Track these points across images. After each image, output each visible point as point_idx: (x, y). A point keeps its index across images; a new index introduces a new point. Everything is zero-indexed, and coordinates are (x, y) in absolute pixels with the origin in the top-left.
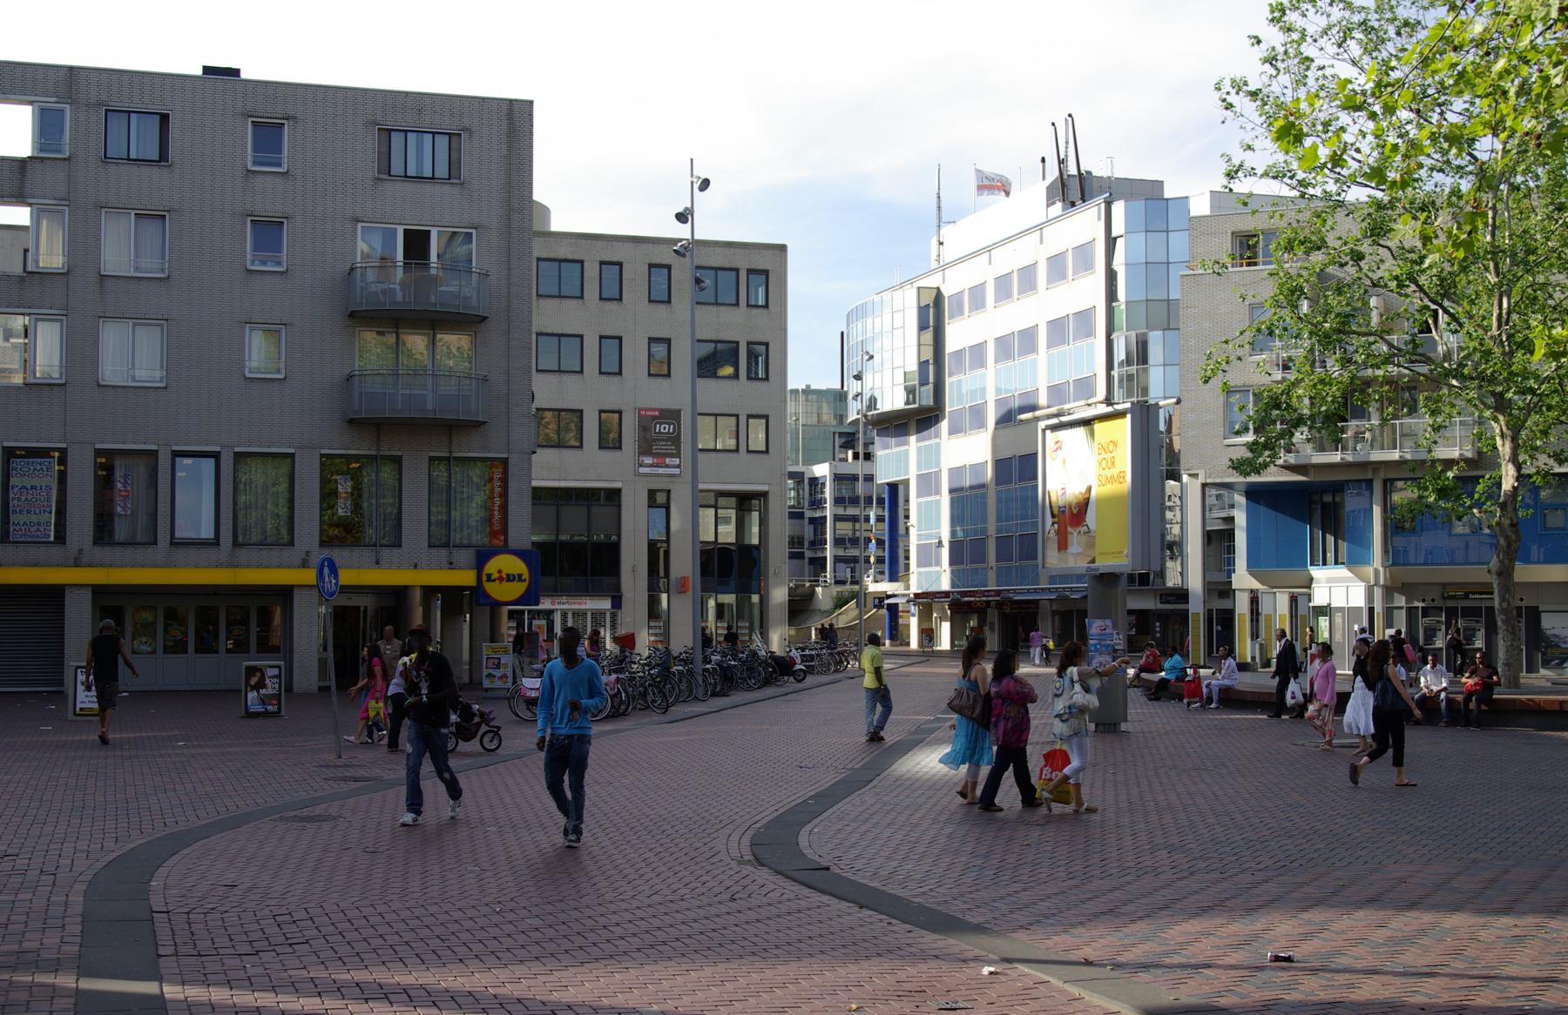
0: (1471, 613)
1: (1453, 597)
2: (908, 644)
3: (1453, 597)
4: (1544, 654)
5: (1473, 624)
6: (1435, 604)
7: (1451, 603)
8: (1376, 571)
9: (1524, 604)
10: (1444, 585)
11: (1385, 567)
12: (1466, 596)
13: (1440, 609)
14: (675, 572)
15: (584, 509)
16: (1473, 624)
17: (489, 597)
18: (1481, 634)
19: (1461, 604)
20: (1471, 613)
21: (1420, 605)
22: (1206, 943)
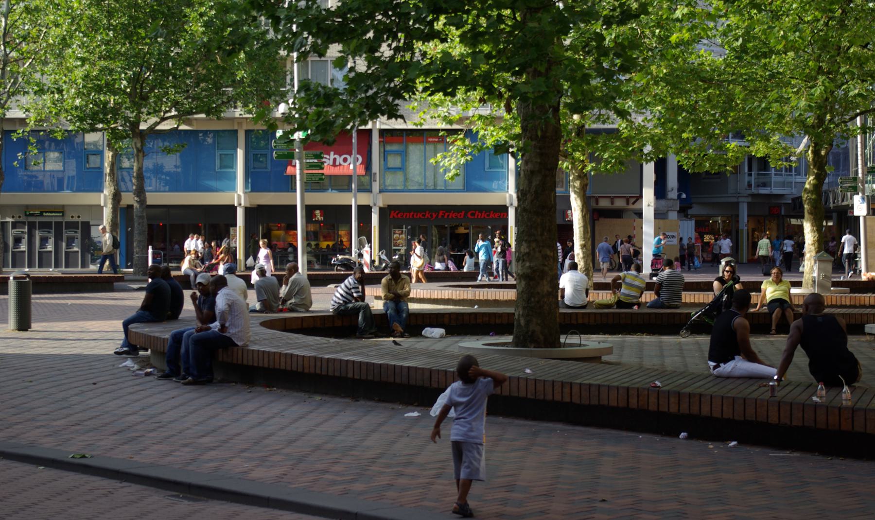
0: (45, 226)
1: (32, 215)
2: (34, 293)
3: (32, 215)
4: (92, 255)
5: (72, 234)
6: (21, 220)
7: (31, 219)
8: (239, 196)
9: (80, 220)
10: (27, 206)
11: (245, 193)
12: (41, 214)
13: (24, 223)
14: (651, 165)
15: (681, 411)
16: (72, 234)
17: (220, 289)
18: (52, 241)
19: (38, 220)
20: (45, 226)
21: (9, 220)
22: (731, 387)
